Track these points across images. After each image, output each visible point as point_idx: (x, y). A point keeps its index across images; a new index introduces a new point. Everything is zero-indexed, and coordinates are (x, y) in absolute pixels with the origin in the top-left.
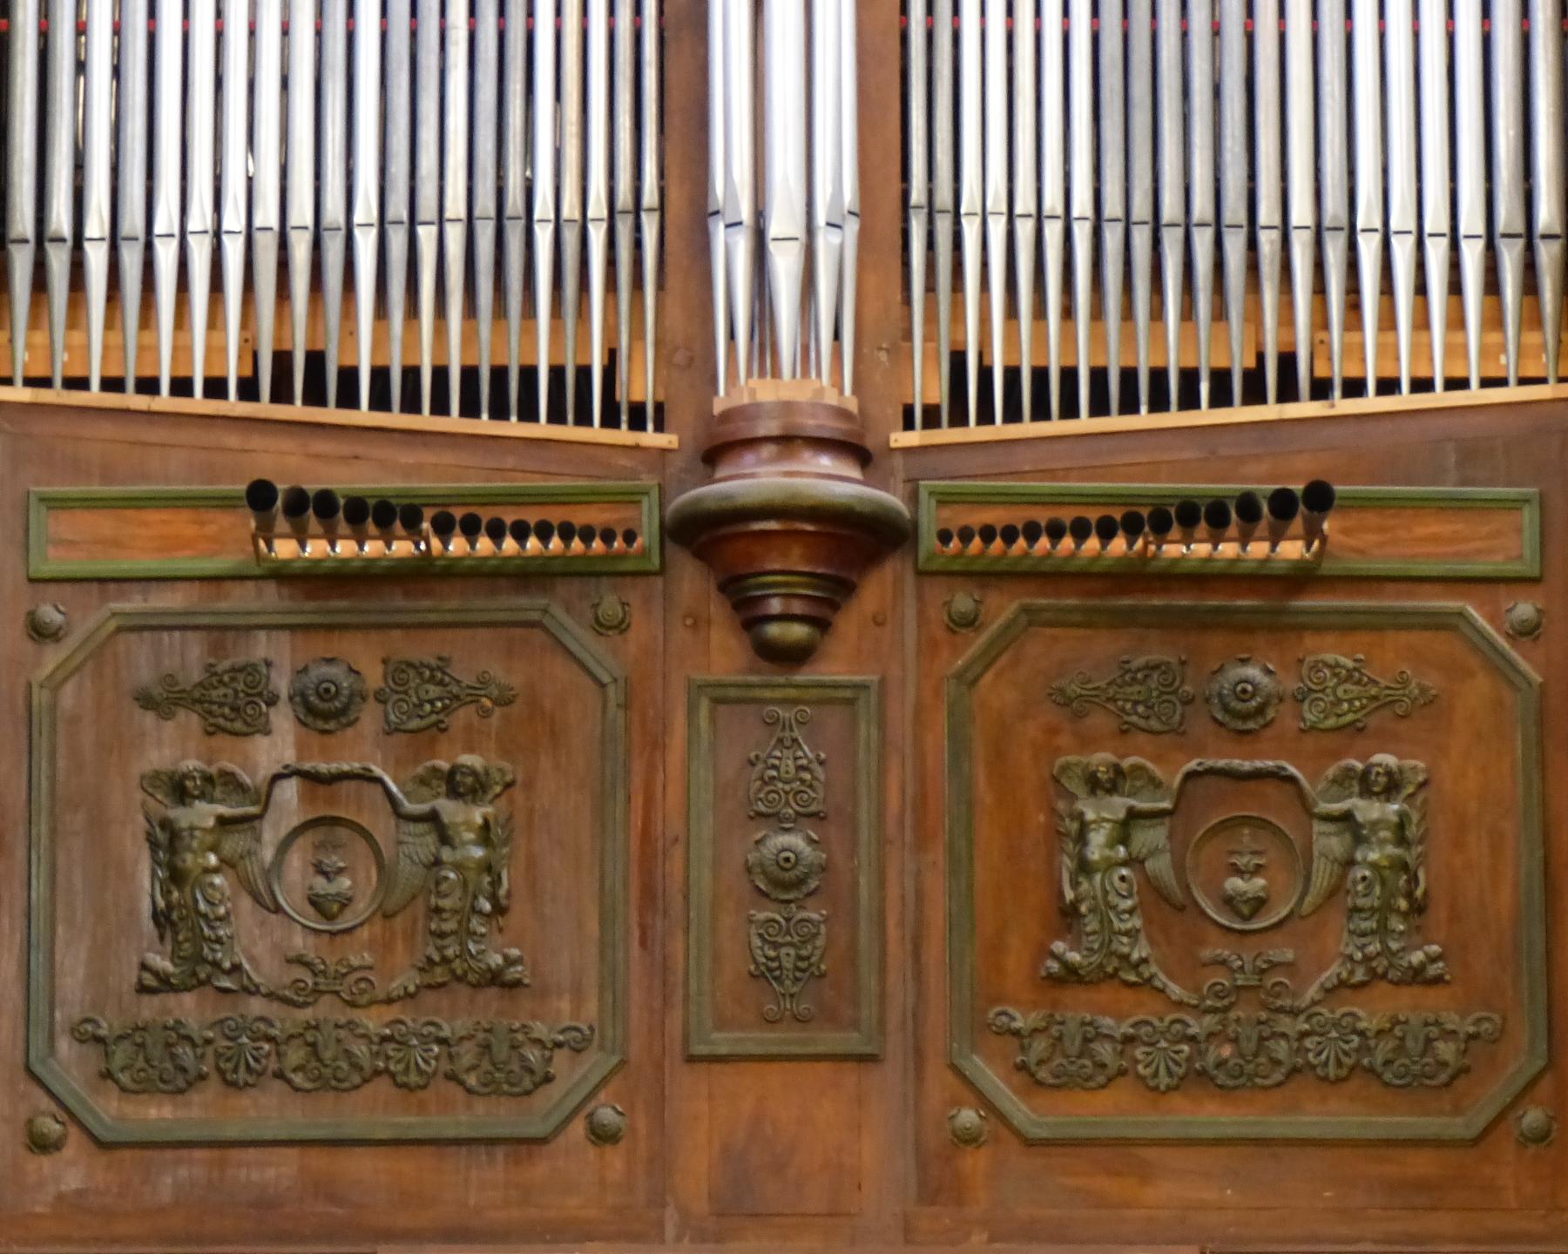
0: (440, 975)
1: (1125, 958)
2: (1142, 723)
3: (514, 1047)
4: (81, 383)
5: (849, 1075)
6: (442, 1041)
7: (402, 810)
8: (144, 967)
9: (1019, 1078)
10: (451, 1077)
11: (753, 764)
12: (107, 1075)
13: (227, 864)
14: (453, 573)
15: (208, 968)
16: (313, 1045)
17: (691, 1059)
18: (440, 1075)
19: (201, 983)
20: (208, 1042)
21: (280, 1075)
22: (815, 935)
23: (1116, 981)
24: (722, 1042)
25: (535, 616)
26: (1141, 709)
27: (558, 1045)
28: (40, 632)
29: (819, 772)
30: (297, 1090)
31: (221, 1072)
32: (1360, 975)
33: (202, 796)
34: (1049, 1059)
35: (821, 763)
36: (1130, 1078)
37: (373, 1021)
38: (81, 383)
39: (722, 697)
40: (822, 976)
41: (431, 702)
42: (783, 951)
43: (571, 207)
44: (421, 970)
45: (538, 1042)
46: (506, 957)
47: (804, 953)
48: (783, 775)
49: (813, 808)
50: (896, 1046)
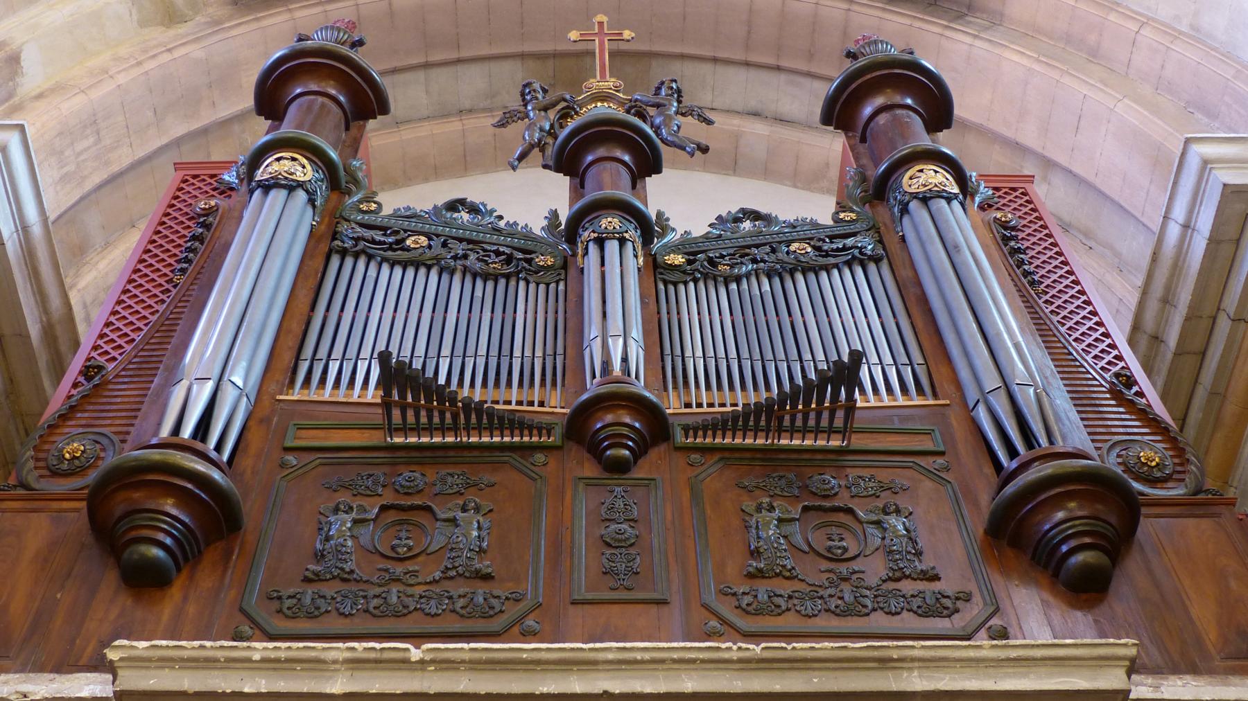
0: (453, 573)
1: (784, 566)
2: (780, 493)
3: (485, 599)
4: (531, 403)
5: (654, 609)
6: (450, 598)
7: (438, 517)
8: (307, 570)
9: (737, 611)
10: (453, 611)
11: (603, 504)
12: (280, 611)
13: (352, 536)
14: (470, 447)
15: (339, 571)
16: (385, 598)
17: (574, 603)
18: (447, 611)
19: (334, 578)
20: (333, 598)
21: (366, 611)
22: (634, 559)
23: (780, 577)
24: (589, 596)
25: (506, 458)
26: (778, 489)
27: (507, 598)
28: (283, 465)
29: (634, 506)
30: (374, 616)
31: (337, 609)
32: (898, 574)
33: (346, 512)
34: (467, 607)
35: (635, 504)
36: (792, 612)
37: (418, 590)
38: (509, 403)
39: (590, 483)
40: (637, 573)
41: (457, 485)
42: (618, 564)
43: (700, 363)
44: (442, 572)
45: (498, 597)
46: (484, 566)
47: (629, 565)
48: (617, 506)
49: (632, 517)
50: (676, 600)
